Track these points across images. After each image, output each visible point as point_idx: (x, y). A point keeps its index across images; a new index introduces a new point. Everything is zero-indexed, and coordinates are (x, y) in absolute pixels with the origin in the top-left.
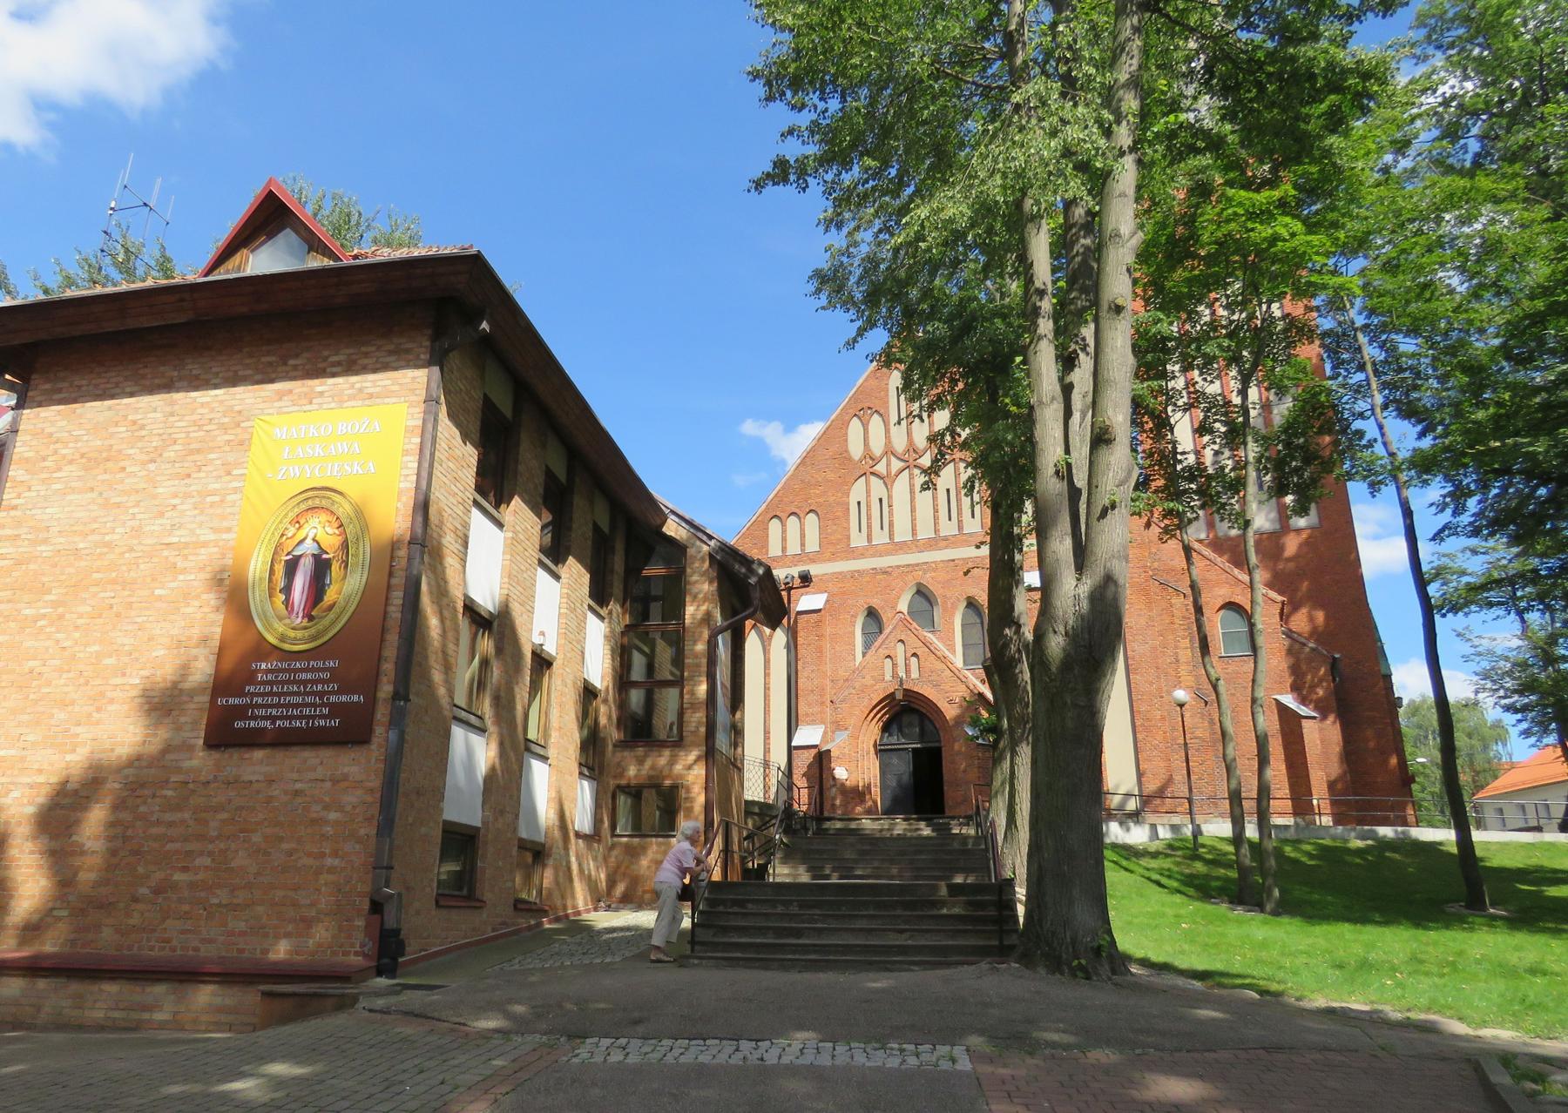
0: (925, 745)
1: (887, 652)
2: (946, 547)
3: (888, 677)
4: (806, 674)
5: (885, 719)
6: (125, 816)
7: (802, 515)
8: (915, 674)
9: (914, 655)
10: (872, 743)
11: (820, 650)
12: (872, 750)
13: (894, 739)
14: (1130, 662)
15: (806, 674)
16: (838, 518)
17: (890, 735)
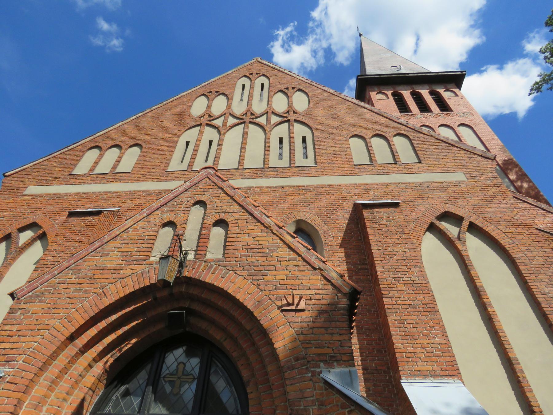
1: (168, 217)
9: (221, 223)
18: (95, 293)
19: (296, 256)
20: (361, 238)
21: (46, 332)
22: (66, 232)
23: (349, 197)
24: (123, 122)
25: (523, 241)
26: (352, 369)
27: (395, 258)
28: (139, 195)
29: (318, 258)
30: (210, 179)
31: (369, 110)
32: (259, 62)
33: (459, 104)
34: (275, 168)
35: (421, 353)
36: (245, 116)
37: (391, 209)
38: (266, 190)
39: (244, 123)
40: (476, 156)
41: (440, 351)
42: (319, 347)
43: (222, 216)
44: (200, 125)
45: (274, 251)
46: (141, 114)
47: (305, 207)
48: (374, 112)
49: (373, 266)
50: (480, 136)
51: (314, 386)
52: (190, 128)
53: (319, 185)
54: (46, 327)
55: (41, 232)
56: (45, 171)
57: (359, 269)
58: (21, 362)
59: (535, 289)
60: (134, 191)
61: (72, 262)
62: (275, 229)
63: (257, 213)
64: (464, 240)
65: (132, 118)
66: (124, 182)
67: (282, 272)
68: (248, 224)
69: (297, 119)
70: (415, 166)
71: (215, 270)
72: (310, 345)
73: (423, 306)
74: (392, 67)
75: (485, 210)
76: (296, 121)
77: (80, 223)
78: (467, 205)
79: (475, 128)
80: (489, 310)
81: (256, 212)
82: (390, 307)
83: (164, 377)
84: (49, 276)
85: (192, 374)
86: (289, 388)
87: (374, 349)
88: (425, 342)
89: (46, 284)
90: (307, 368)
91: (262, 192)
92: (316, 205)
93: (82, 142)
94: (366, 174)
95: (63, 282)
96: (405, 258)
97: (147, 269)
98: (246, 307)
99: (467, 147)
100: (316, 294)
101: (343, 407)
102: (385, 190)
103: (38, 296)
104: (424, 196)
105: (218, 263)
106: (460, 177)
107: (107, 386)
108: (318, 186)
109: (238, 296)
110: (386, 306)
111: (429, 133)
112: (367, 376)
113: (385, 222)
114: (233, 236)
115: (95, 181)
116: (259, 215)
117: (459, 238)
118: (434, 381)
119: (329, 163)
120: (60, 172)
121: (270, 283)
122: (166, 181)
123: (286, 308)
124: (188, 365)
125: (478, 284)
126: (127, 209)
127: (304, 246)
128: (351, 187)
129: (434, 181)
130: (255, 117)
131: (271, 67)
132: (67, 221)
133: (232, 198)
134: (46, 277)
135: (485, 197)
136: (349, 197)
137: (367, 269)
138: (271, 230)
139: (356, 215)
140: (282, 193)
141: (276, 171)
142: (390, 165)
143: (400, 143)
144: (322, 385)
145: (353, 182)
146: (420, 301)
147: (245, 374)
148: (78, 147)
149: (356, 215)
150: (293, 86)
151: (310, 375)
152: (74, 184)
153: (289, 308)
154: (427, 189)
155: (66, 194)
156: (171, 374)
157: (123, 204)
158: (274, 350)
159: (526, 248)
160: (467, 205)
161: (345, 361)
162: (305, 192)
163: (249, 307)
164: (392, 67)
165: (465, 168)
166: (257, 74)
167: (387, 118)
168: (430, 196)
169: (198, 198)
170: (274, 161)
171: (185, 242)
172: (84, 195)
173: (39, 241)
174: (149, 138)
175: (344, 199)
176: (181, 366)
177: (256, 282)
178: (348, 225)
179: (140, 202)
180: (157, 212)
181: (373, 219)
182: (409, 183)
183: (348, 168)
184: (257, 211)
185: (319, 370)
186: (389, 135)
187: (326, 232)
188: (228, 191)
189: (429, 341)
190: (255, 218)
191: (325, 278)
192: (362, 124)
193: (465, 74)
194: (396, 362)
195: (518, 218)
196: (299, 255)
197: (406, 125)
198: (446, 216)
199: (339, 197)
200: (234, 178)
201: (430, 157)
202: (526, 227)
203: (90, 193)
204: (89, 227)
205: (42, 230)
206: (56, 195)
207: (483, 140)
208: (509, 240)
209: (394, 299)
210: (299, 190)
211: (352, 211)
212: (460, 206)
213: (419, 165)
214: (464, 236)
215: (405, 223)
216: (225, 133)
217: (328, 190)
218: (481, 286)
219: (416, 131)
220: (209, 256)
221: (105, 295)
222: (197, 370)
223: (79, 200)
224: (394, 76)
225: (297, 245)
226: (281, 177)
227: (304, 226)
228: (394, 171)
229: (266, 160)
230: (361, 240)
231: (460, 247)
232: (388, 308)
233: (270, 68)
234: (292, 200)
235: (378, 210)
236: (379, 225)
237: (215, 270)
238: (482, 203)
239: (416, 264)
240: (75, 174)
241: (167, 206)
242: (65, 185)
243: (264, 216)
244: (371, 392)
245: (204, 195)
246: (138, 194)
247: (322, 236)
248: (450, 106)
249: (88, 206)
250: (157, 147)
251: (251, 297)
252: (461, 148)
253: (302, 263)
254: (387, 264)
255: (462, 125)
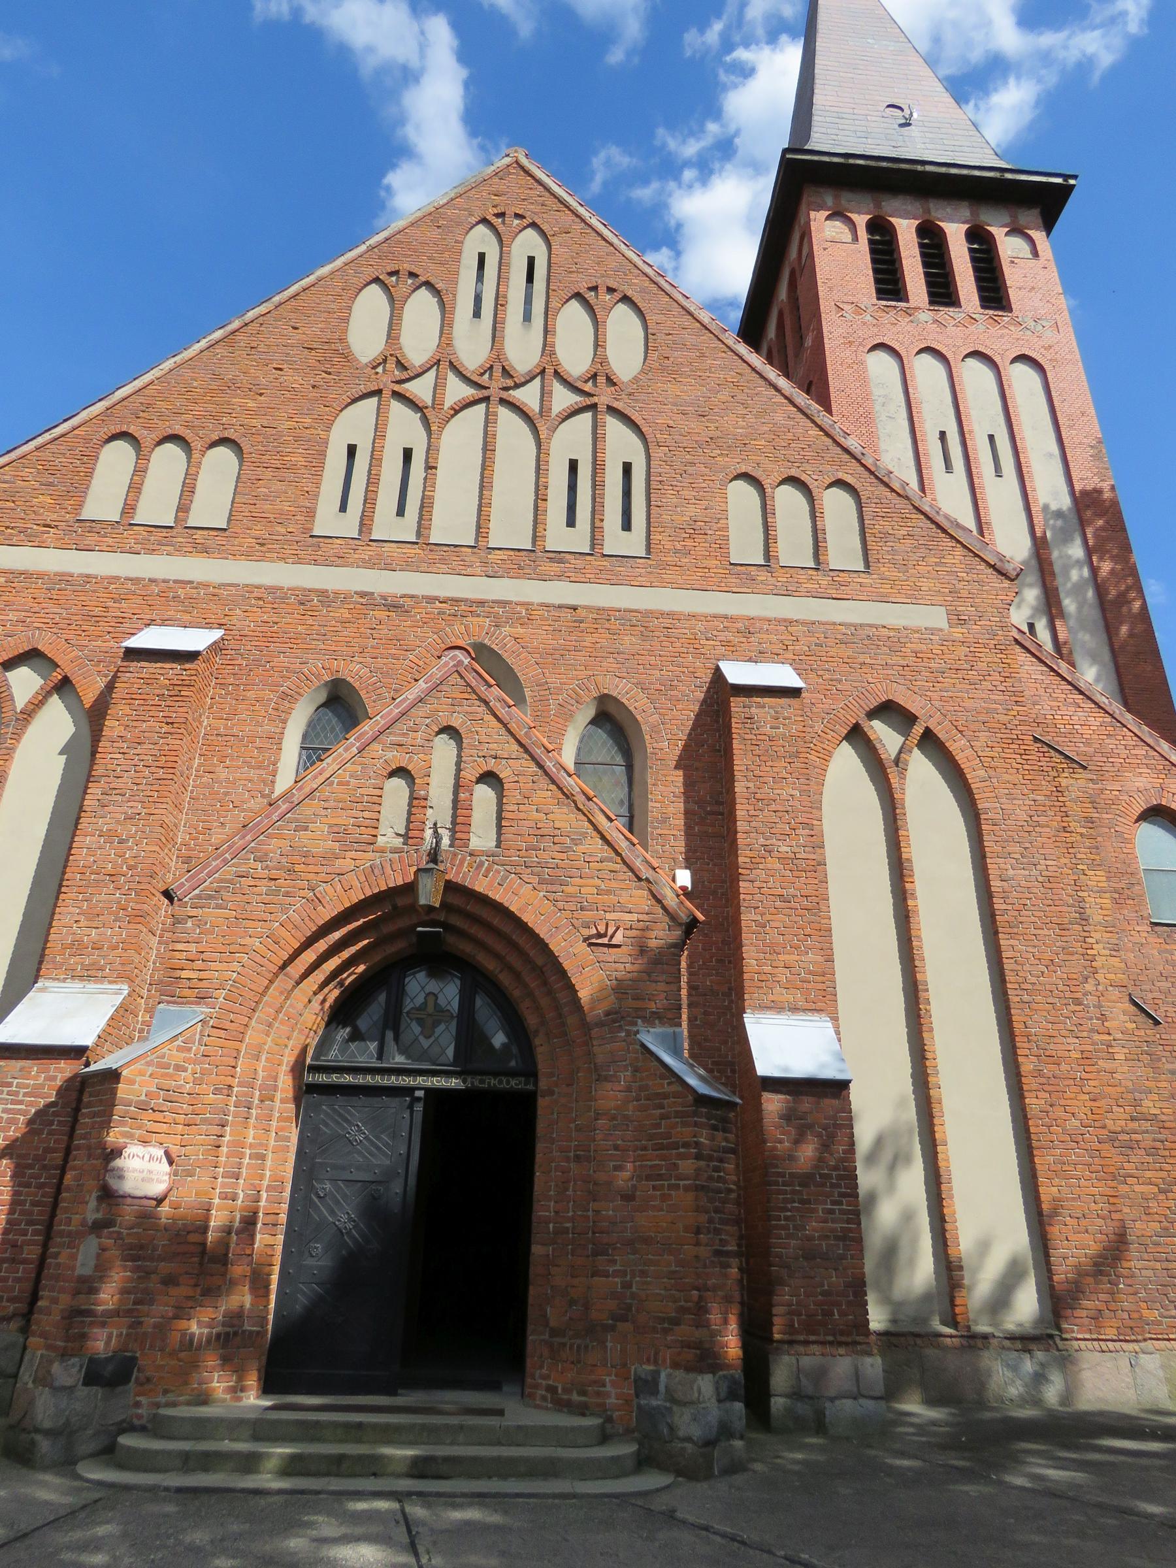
0: (475, 1082)
1: (397, 758)
2: (559, 577)
3: (389, 836)
4: (104, 824)
5: (349, 978)
6: (110, 1030)
7: (197, 445)
8: (482, 837)
9: (488, 778)
10: (289, 1058)
11: (168, 764)
12: (285, 1083)
13: (366, 1053)
14: (999, 904)
15: (104, 824)
16: (292, 468)
17: (356, 1036)
18: (303, 898)
19: (613, 855)
20: (720, 746)
21: (244, 957)
22: (134, 696)
23: (709, 647)
24: (177, 359)
25: (1006, 777)
26: (677, 1029)
27: (773, 807)
28: (260, 599)
29: (647, 862)
30: (462, 677)
31: (786, 398)
32: (522, 168)
33: (1033, 288)
34: (560, 552)
35: (783, 975)
36: (487, 375)
37: (784, 701)
38: (539, 613)
39: (486, 399)
40: (983, 566)
41: (810, 973)
42: (638, 999)
43: (491, 765)
44: (378, 392)
45: (578, 842)
46: (218, 334)
47: (618, 666)
48: (795, 406)
49: (731, 818)
50: (1056, 403)
51: (628, 1048)
52: (355, 401)
53: (651, 612)
54: (241, 949)
55: (60, 677)
56: (13, 502)
57: (710, 813)
58: (221, 999)
59: (993, 871)
60: (247, 586)
61: (249, 838)
62: (580, 799)
63: (551, 765)
64: (905, 767)
65: (197, 347)
66: (216, 555)
67: (590, 881)
68: (535, 786)
69: (615, 405)
70: (855, 580)
71: (488, 870)
72: (625, 996)
73: (800, 899)
74: (889, 106)
75: (961, 704)
76: (611, 410)
77: (158, 677)
78: (932, 689)
79: (1049, 375)
80: (910, 902)
81: (548, 763)
82: (749, 897)
83: (408, 1013)
84: (218, 861)
85: (448, 1010)
86: (596, 1049)
87: (712, 957)
88: (791, 958)
89: (216, 875)
90: (620, 1026)
91: (530, 617)
92: (640, 662)
93: (84, 415)
94: (750, 590)
95: (244, 874)
96: (789, 809)
97: (378, 861)
98: (538, 935)
99: (970, 540)
100: (639, 921)
101: (662, 1077)
102: (783, 637)
103: (210, 897)
104: (855, 661)
105: (491, 859)
106: (935, 617)
107: (328, 1024)
108: (648, 614)
109: (525, 918)
110: (742, 896)
111: (904, 489)
112: (695, 999)
113: (767, 729)
114: (511, 808)
115: (147, 547)
116: (554, 770)
117: (897, 761)
118: (794, 1017)
119: (677, 551)
120: (51, 509)
121: (572, 899)
122: (316, 562)
123: (594, 941)
124: (440, 996)
125: (904, 856)
126: (238, 633)
127: (627, 839)
128: (716, 623)
129: (884, 623)
130: (512, 384)
131: (555, 197)
132: (128, 670)
133: (505, 725)
134: (214, 864)
135: (970, 672)
136: (709, 647)
137: (722, 814)
138: (575, 802)
139: (717, 693)
140: (573, 624)
141: (561, 561)
142: (802, 572)
143: (836, 504)
144: (638, 1047)
145: (721, 610)
146: (799, 890)
147: (531, 1020)
148: (76, 432)
149: (717, 693)
150: (614, 285)
151: (623, 1034)
152: (97, 548)
153: (600, 941)
154: (866, 642)
155: (88, 576)
156: (419, 1009)
157: (227, 618)
158: (579, 999)
159: (1006, 791)
160: (932, 689)
161: (670, 1019)
162: (621, 627)
163: (542, 936)
164: (889, 106)
165: (952, 599)
166: (518, 216)
167: (822, 429)
168: (868, 661)
169: (444, 719)
170: (558, 537)
171: (431, 810)
172: (129, 585)
173: (56, 696)
174: (254, 422)
175: (698, 654)
176: (431, 1000)
177: (552, 896)
178: (698, 716)
179: (265, 618)
180: (375, 746)
181: (746, 720)
182: (834, 624)
183: (715, 571)
184: (550, 759)
185: (635, 1029)
186: (816, 483)
187: (655, 729)
188: (499, 710)
189: (798, 958)
190: (546, 773)
191: (654, 896)
192: (763, 443)
193: (1074, 186)
194: (743, 987)
195: (1014, 727)
196: (618, 854)
197: (860, 456)
198: (888, 710)
199: (688, 646)
200: (469, 571)
201: (890, 557)
202: (1022, 747)
203: (144, 579)
204: (180, 688)
205: (58, 670)
206: (64, 578)
207: (1059, 414)
208: (982, 773)
209: (757, 884)
210: (608, 620)
211: (711, 682)
212: (917, 690)
213: (865, 579)
214: (907, 758)
215: (803, 734)
216: (441, 428)
217: (668, 625)
218: (909, 860)
219: (877, 477)
220: (475, 843)
221: (320, 902)
222: (455, 1005)
223: (122, 596)
224: (884, 164)
225: (614, 835)
226: (572, 579)
227: (612, 709)
228: (809, 590)
229: (540, 528)
230: (719, 751)
231: (894, 781)
232: (744, 900)
233: (550, 201)
234: (592, 645)
235: (759, 700)
236: (755, 735)
237: (488, 870)
238: (961, 686)
239: (806, 821)
240: (94, 521)
241: (390, 733)
242: (76, 549)
243: (562, 772)
244: (698, 1022)
245: (455, 714)
246: (255, 595)
247: (647, 737)
248: (1010, 291)
249: (148, 617)
250: (278, 457)
251: (544, 920)
252: (958, 541)
253: (619, 867)
254: (757, 819)
255: (1023, 358)
